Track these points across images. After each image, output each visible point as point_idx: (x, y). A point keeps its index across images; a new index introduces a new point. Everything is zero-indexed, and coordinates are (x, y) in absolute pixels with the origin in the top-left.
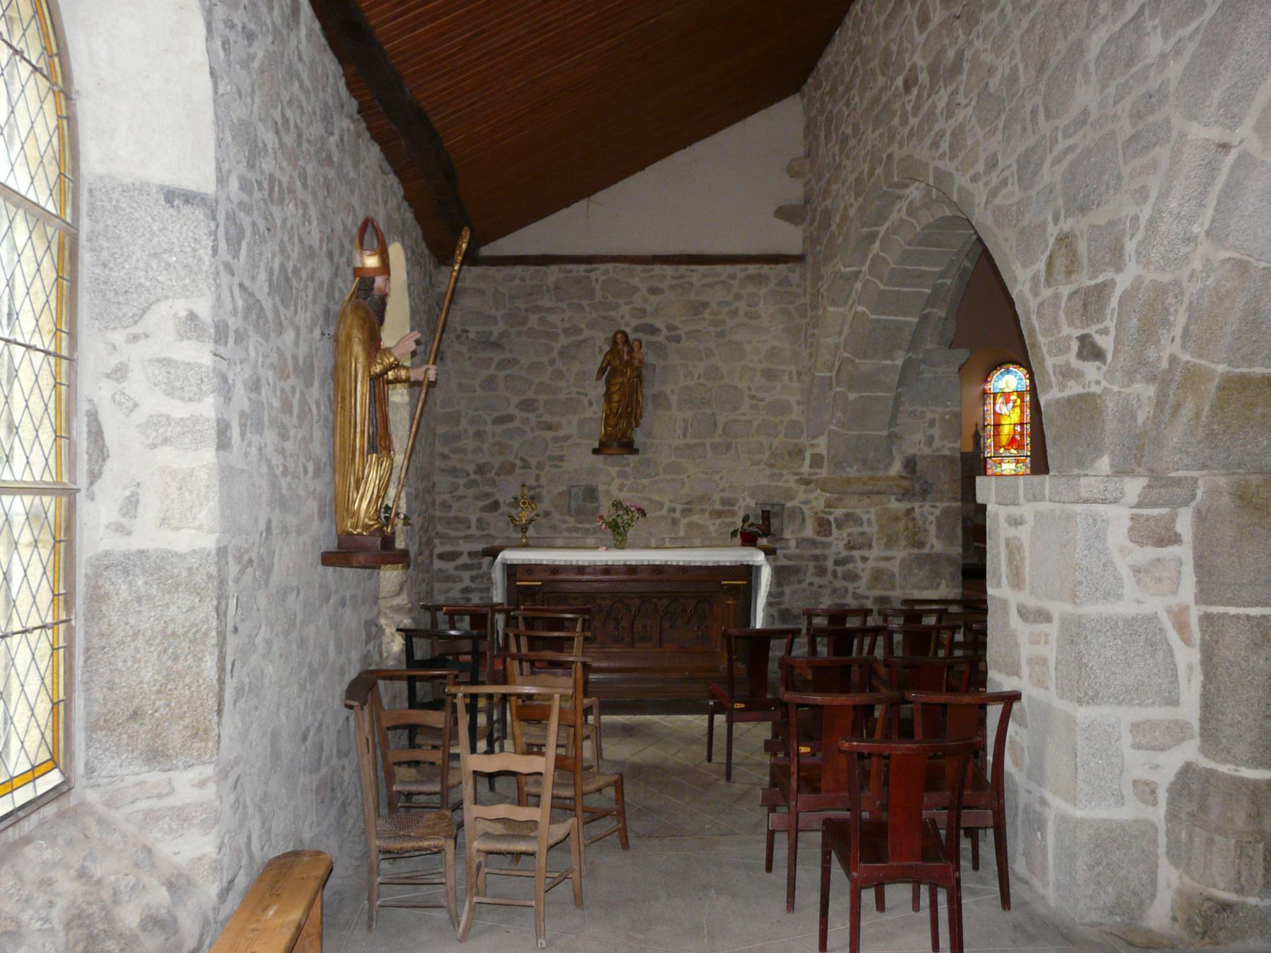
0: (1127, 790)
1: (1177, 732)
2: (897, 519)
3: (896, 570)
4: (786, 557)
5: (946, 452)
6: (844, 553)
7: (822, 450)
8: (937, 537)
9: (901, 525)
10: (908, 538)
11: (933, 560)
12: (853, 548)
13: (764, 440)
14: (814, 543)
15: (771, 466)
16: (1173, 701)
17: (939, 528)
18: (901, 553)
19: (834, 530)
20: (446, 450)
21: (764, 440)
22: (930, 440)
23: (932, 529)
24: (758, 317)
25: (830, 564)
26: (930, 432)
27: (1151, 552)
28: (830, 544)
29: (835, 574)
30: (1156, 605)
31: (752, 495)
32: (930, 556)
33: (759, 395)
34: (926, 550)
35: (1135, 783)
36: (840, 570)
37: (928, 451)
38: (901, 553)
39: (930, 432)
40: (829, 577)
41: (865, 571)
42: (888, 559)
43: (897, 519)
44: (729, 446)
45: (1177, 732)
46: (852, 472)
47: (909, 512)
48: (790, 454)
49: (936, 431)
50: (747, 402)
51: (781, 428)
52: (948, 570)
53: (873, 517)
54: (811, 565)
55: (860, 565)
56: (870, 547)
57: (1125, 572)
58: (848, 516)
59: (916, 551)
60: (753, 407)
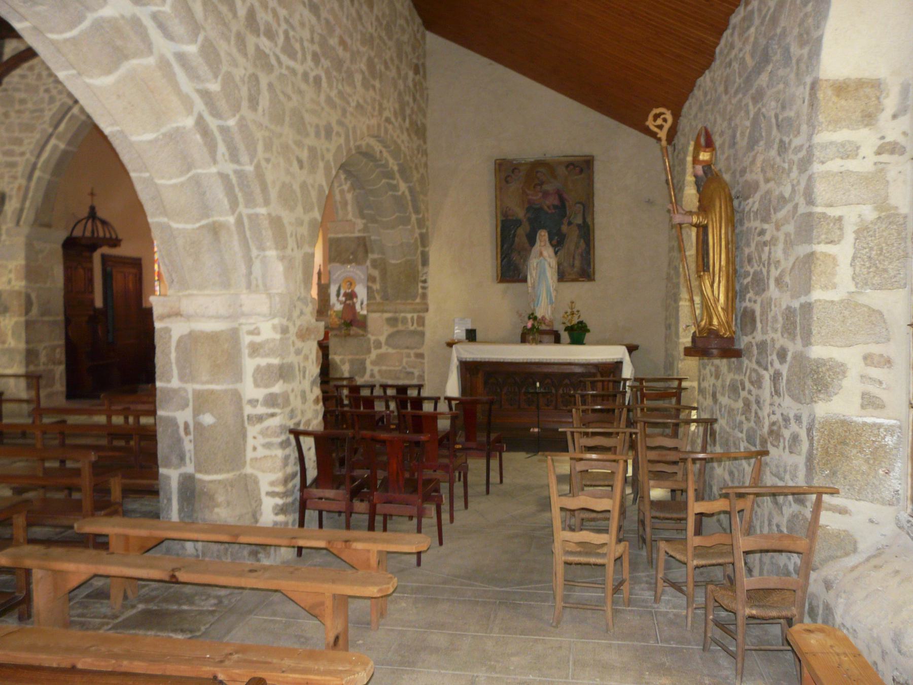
22: (9, 282)
23: (10, 333)
34: (6, 346)
37: (8, 288)
49: (12, 276)
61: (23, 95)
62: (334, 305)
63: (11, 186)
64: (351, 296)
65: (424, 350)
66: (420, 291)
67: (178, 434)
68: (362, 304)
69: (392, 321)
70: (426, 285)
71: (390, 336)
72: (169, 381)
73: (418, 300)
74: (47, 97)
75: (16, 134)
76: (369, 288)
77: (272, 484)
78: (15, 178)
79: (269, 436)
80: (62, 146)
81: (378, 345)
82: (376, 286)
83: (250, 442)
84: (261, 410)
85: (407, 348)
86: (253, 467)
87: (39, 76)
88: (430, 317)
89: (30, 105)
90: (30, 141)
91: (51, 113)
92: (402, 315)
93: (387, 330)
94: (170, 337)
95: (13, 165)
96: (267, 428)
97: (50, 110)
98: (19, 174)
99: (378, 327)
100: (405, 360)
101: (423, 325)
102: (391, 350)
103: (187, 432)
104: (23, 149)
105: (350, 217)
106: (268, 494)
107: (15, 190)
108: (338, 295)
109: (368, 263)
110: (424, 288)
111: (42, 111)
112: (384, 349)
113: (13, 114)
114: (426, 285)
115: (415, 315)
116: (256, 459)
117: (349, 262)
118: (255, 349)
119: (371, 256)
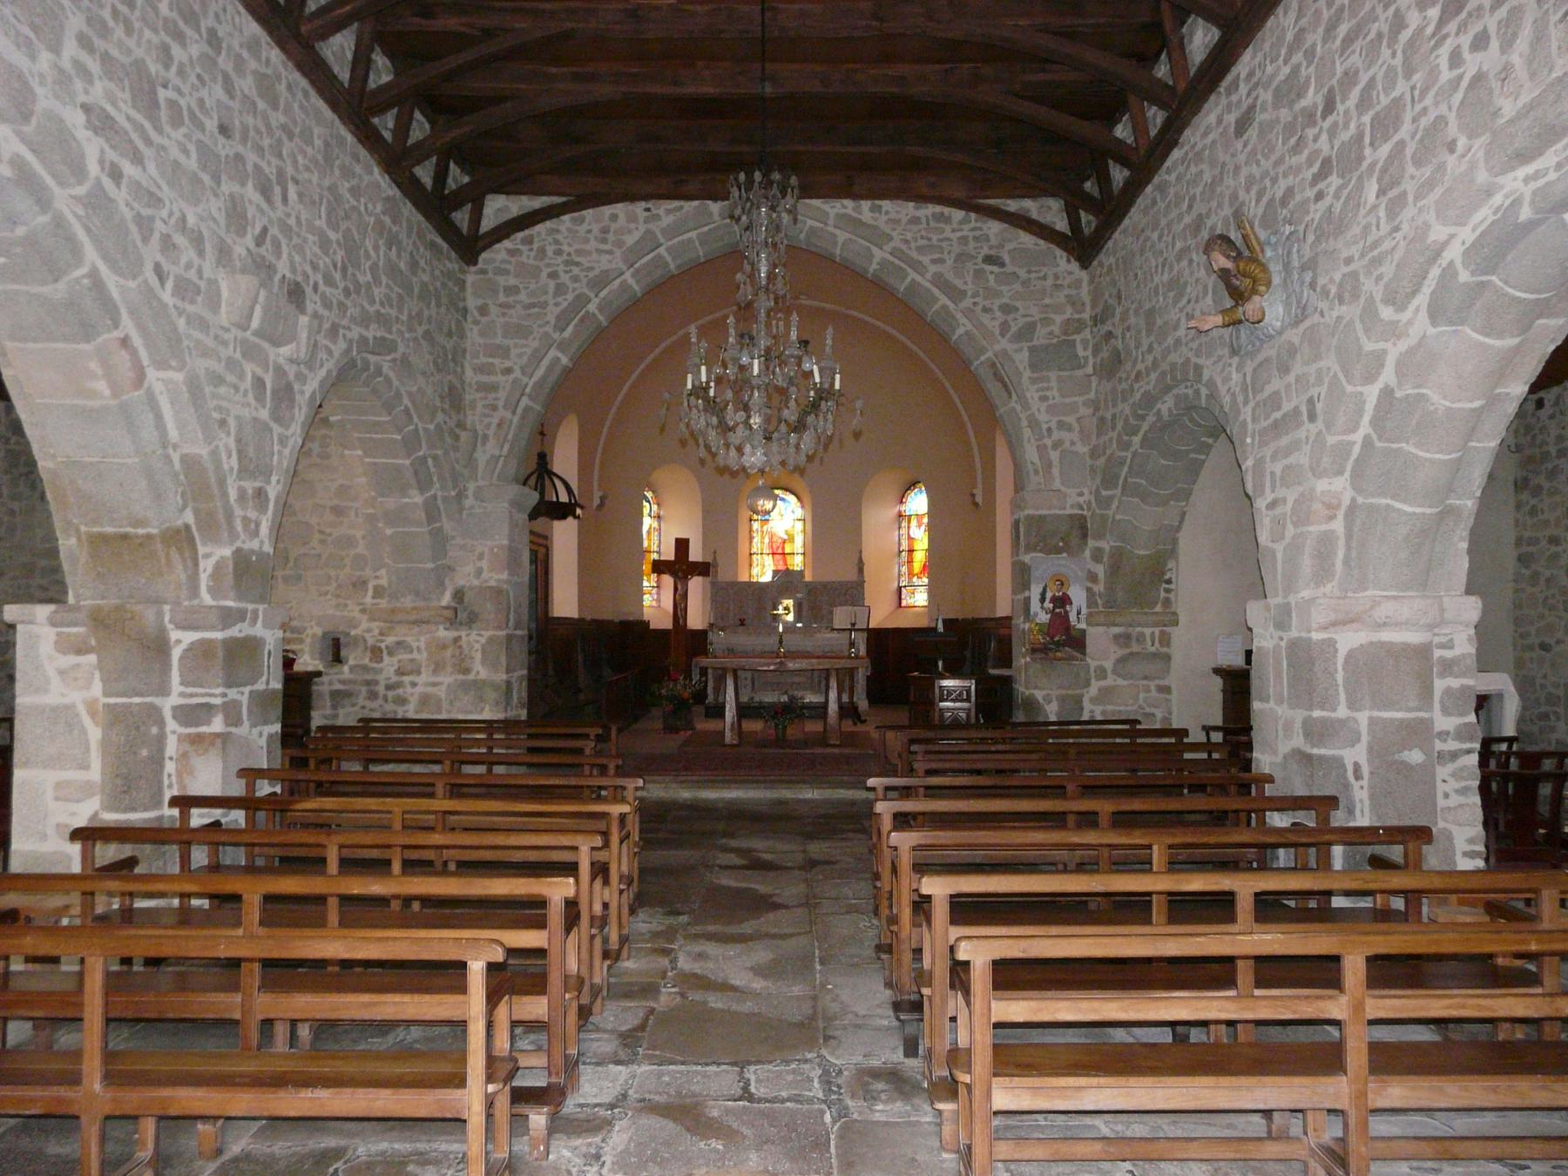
0: (51, 831)
1: (86, 790)
2: (444, 647)
3: (443, 695)
4: (340, 682)
5: (493, 583)
6: (395, 679)
7: (384, 582)
8: (483, 662)
9: (449, 653)
10: (454, 665)
11: (478, 685)
12: (403, 674)
13: (333, 573)
14: (365, 668)
15: (338, 596)
16: (85, 767)
17: (484, 652)
18: (447, 679)
19: (386, 657)
20: (44, 582)
21: (333, 573)
22: (479, 572)
23: (478, 656)
24: (328, 457)
25: (381, 689)
26: (479, 564)
27: (72, 659)
28: (381, 670)
29: (386, 699)
30: (76, 697)
31: (318, 624)
32: (475, 682)
33: (328, 530)
34: (471, 677)
35: (58, 825)
36: (391, 694)
37: (476, 583)
38: (447, 679)
39: (479, 564)
40: (380, 701)
41: (413, 694)
42: (435, 684)
43: (444, 647)
44: (299, 578)
45: (86, 790)
46: (408, 602)
47: (457, 640)
48: (354, 585)
49: (484, 564)
50: (317, 536)
51: (347, 561)
52: (491, 695)
53: (423, 646)
54: (364, 689)
55: (409, 690)
56: (419, 673)
57: (51, 673)
58: (399, 643)
59: (461, 677)
60: (322, 542)
61: (512, 281)
62: (1036, 614)
63: (487, 420)
64: (1063, 601)
65: (1171, 680)
66: (1163, 594)
67: (1345, 778)
68: (1079, 613)
69: (1123, 640)
70: (1172, 586)
71: (1121, 661)
72: (1334, 710)
73: (1158, 608)
74: (552, 284)
75: (499, 340)
76: (1089, 590)
77: (1471, 841)
78: (494, 408)
79: (1463, 778)
80: (565, 360)
81: (1102, 673)
82: (1099, 588)
83: (1441, 788)
84: (1453, 745)
85: (1146, 678)
86: (1445, 820)
87: (542, 252)
88: (1179, 635)
89: (523, 297)
90: (521, 349)
91: (558, 310)
92: (1139, 629)
93: (1116, 652)
94: (1336, 651)
95: (493, 388)
96: (1461, 769)
97: (556, 305)
98: (501, 404)
99: (1101, 643)
100: (1142, 695)
101: (1168, 645)
102: (1120, 682)
103: (1358, 777)
104: (508, 364)
105: (1057, 484)
106: (1465, 854)
107: (493, 427)
108: (1043, 600)
109: (1087, 553)
110: (1168, 591)
111: (544, 305)
112: (1110, 681)
113: (494, 310)
114: (1172, 586)
115: (1157, 631)
116: (1449, 809)
117: (1059, 551)
118: (1448, 667)
119: (1091, 543)
